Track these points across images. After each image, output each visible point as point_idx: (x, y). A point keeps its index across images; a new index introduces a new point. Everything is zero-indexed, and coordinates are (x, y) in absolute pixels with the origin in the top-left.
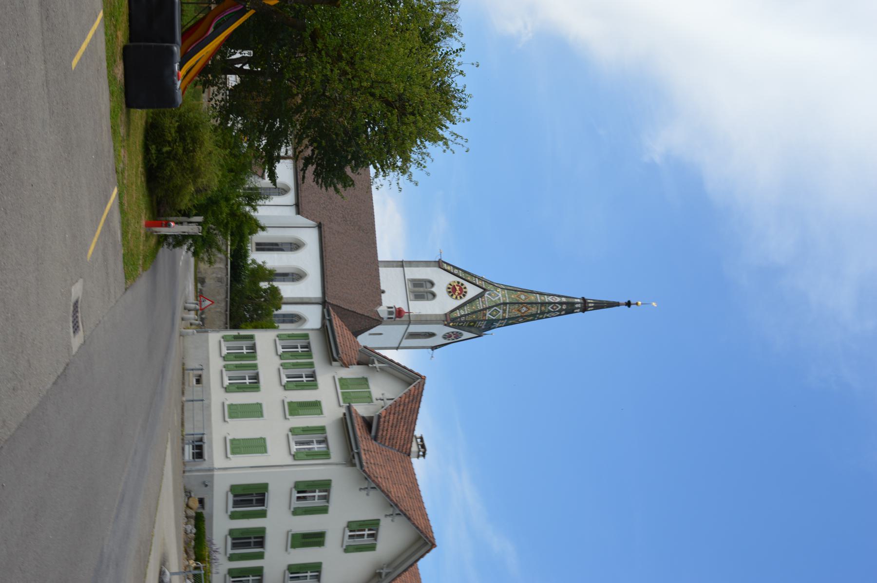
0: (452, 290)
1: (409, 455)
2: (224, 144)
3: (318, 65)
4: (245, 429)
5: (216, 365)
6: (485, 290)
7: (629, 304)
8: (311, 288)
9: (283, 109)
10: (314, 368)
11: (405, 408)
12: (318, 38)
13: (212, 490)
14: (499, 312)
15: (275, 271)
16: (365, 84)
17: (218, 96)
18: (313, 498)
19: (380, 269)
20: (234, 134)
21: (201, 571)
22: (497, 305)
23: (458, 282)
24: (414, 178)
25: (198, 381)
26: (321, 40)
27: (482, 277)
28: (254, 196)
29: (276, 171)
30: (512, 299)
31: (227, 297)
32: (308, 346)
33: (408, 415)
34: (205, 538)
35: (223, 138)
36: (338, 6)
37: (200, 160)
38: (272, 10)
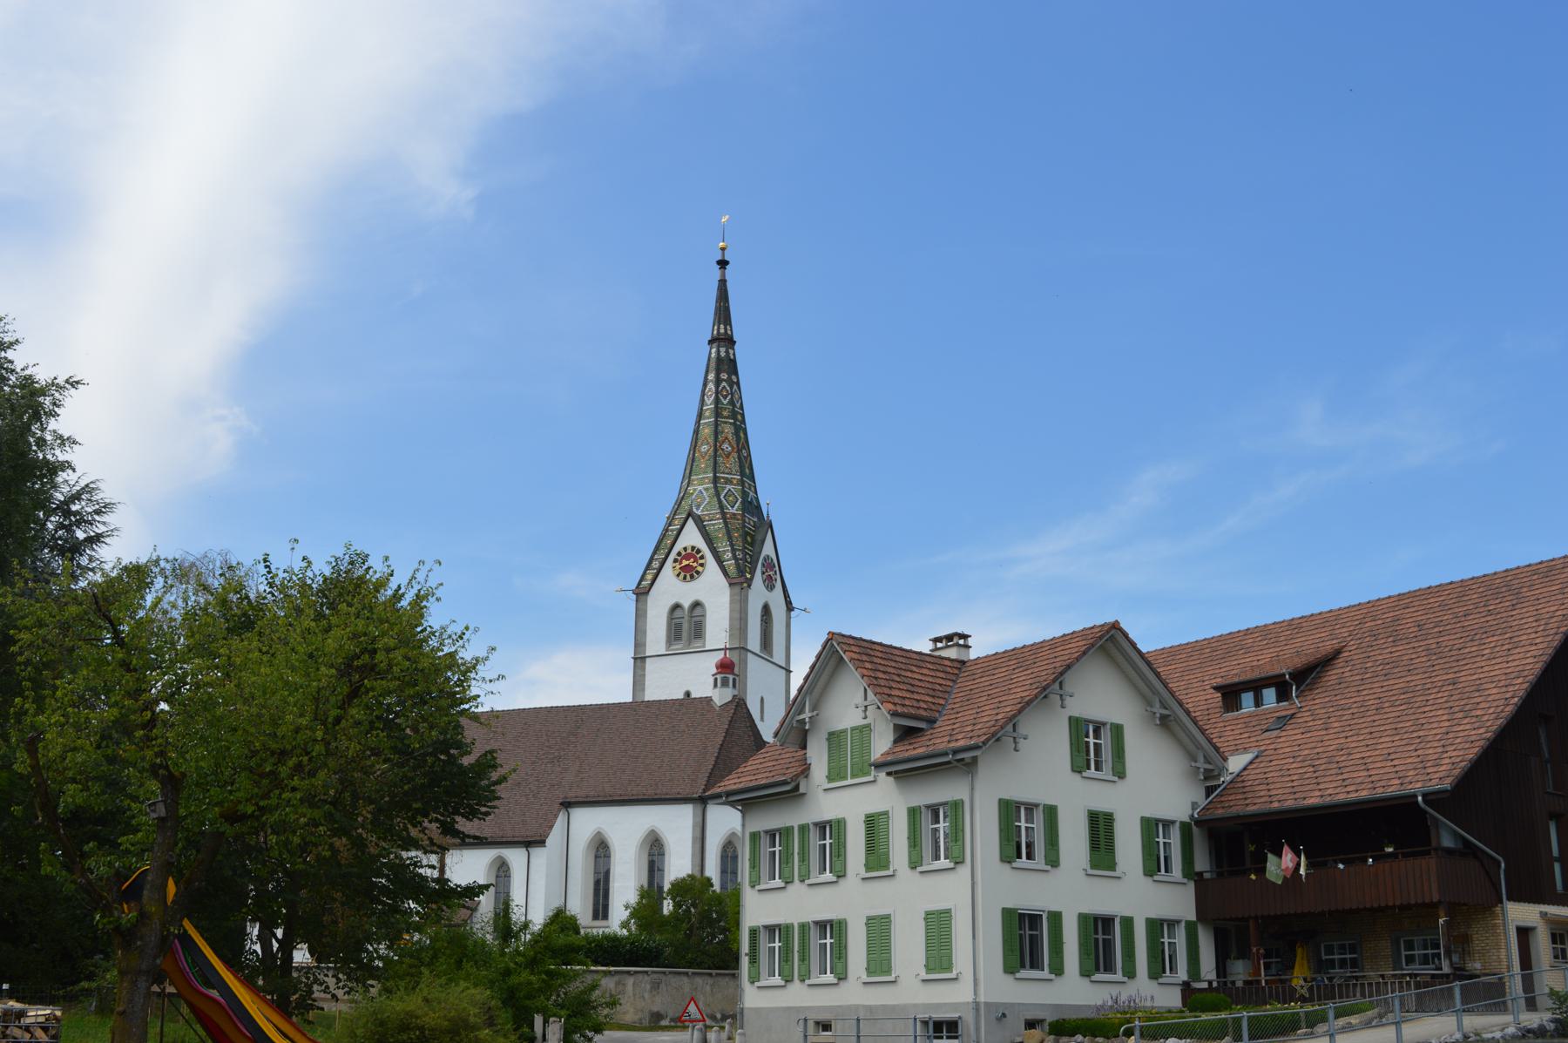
0: (689, 572)
1: (963, 663)
2: (412, 975)
3: (283, 813)
4: (909, 947)
5: (800, 996)
6: (690, 514)
7: (723, 264)
8: (675, 823)
9: (355, 870)
10: (808, 824)
11: (882, 668)
12: (238, 811)
13: (1012, 1005)
14: (730, 490)
15: (642, 886)
16: (319, 735)
17: (329, 984)
18: (1030, 830)
19: (646, 700)
20: (396, 958)
21: (1135, 1026)
22: (718, 494)
23: (675, 561)
24: (482, 654)
25: (826, 1027)
26: (240, 807)
27: (668, 518)
28: (504, 926)
29: (464, 883)
30: (707, 466)
31: (687, 973)
32: (772, 834)
33: (893, 664)
34: (1093, 1019)
35: (401, 978)
36: (184, 775)
37: (438, 1017)
38: (186, 889)
